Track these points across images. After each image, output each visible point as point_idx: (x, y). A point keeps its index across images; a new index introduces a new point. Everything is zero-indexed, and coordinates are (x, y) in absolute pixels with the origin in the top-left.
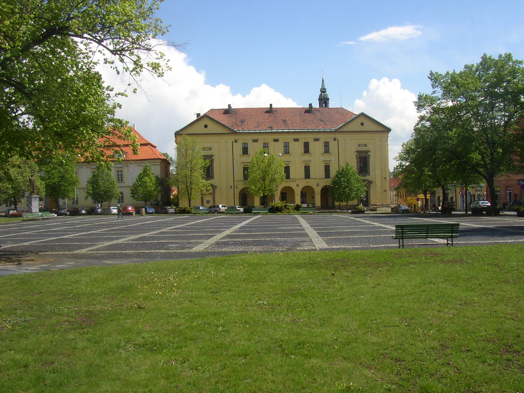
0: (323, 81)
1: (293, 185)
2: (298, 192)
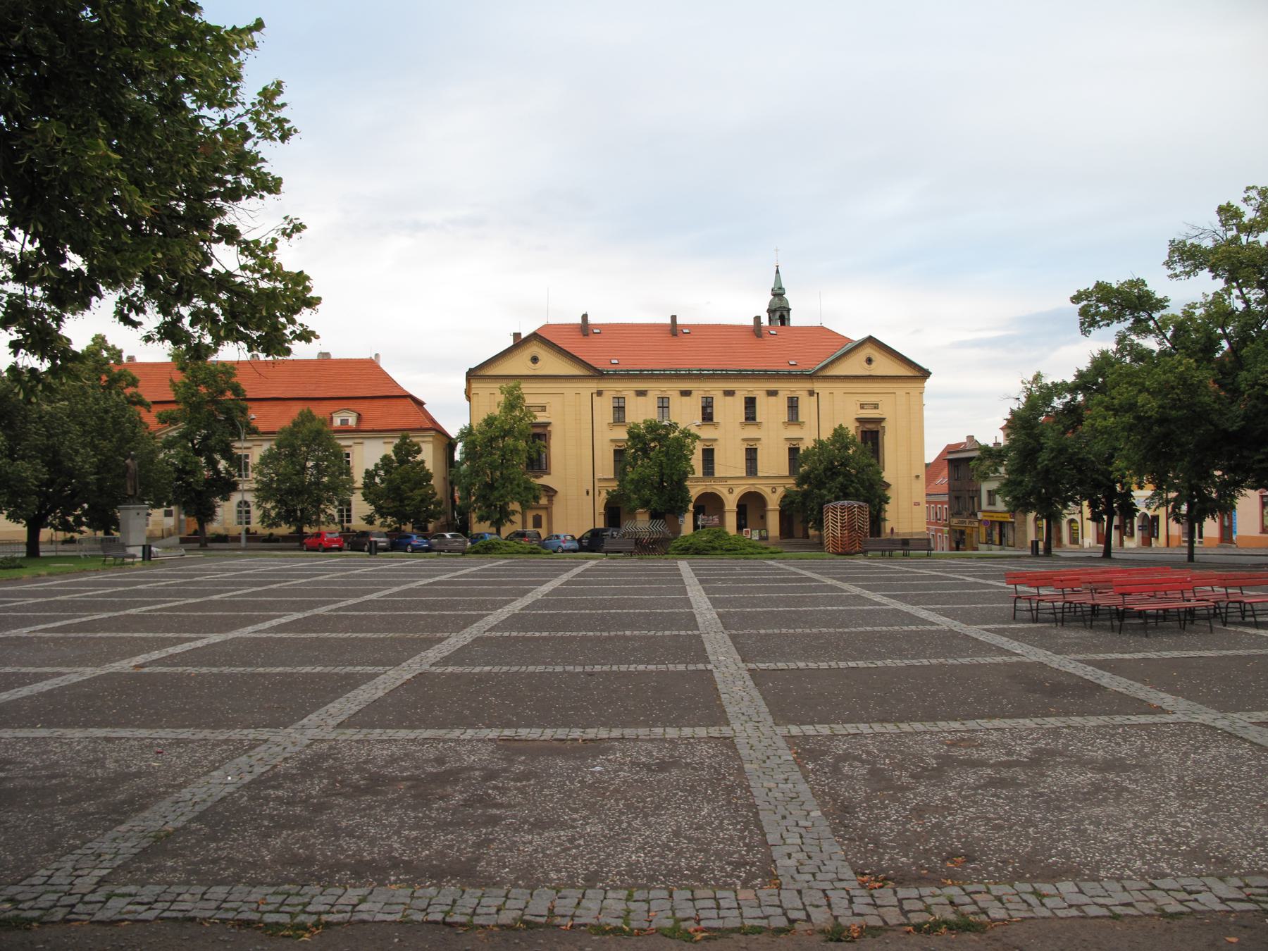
0: (778, 272)
2: (731, 503)
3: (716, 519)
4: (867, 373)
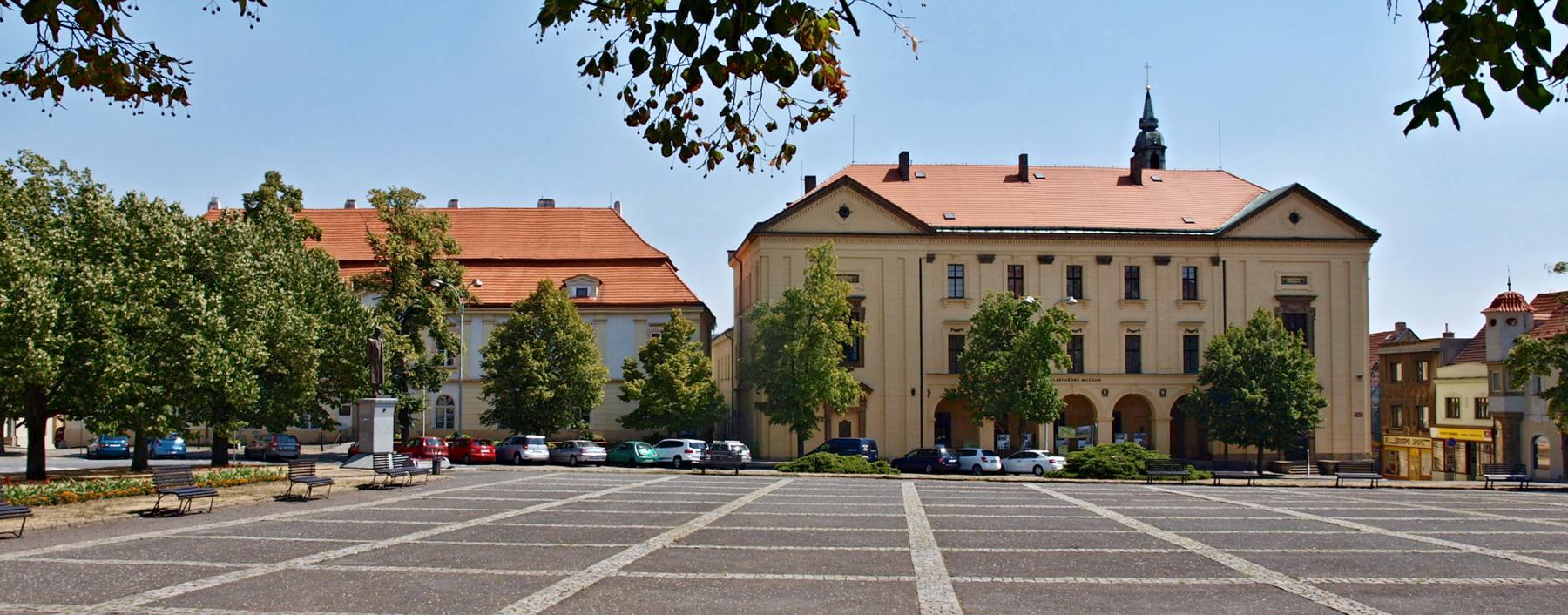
0: (1148, 97)
1: (1090, 391)
2: (1105, 410)
3: (1478, 445)
4: (1292, 235)
